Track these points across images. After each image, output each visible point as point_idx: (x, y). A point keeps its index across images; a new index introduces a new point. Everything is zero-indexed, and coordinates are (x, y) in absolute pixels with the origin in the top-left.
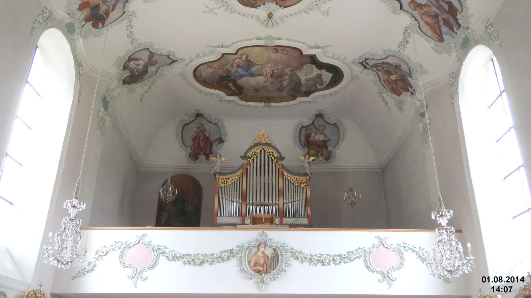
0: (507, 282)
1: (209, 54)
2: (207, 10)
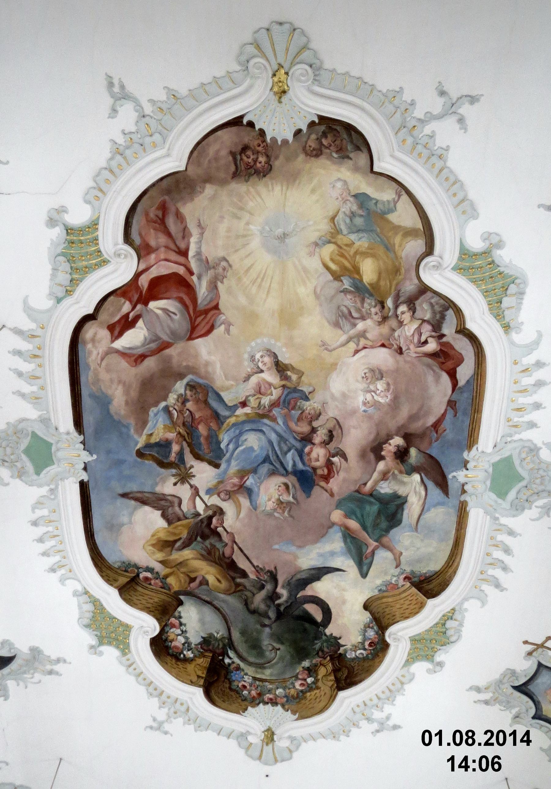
0: (487, 744)
1: (182, 597)
2: (155, 725)
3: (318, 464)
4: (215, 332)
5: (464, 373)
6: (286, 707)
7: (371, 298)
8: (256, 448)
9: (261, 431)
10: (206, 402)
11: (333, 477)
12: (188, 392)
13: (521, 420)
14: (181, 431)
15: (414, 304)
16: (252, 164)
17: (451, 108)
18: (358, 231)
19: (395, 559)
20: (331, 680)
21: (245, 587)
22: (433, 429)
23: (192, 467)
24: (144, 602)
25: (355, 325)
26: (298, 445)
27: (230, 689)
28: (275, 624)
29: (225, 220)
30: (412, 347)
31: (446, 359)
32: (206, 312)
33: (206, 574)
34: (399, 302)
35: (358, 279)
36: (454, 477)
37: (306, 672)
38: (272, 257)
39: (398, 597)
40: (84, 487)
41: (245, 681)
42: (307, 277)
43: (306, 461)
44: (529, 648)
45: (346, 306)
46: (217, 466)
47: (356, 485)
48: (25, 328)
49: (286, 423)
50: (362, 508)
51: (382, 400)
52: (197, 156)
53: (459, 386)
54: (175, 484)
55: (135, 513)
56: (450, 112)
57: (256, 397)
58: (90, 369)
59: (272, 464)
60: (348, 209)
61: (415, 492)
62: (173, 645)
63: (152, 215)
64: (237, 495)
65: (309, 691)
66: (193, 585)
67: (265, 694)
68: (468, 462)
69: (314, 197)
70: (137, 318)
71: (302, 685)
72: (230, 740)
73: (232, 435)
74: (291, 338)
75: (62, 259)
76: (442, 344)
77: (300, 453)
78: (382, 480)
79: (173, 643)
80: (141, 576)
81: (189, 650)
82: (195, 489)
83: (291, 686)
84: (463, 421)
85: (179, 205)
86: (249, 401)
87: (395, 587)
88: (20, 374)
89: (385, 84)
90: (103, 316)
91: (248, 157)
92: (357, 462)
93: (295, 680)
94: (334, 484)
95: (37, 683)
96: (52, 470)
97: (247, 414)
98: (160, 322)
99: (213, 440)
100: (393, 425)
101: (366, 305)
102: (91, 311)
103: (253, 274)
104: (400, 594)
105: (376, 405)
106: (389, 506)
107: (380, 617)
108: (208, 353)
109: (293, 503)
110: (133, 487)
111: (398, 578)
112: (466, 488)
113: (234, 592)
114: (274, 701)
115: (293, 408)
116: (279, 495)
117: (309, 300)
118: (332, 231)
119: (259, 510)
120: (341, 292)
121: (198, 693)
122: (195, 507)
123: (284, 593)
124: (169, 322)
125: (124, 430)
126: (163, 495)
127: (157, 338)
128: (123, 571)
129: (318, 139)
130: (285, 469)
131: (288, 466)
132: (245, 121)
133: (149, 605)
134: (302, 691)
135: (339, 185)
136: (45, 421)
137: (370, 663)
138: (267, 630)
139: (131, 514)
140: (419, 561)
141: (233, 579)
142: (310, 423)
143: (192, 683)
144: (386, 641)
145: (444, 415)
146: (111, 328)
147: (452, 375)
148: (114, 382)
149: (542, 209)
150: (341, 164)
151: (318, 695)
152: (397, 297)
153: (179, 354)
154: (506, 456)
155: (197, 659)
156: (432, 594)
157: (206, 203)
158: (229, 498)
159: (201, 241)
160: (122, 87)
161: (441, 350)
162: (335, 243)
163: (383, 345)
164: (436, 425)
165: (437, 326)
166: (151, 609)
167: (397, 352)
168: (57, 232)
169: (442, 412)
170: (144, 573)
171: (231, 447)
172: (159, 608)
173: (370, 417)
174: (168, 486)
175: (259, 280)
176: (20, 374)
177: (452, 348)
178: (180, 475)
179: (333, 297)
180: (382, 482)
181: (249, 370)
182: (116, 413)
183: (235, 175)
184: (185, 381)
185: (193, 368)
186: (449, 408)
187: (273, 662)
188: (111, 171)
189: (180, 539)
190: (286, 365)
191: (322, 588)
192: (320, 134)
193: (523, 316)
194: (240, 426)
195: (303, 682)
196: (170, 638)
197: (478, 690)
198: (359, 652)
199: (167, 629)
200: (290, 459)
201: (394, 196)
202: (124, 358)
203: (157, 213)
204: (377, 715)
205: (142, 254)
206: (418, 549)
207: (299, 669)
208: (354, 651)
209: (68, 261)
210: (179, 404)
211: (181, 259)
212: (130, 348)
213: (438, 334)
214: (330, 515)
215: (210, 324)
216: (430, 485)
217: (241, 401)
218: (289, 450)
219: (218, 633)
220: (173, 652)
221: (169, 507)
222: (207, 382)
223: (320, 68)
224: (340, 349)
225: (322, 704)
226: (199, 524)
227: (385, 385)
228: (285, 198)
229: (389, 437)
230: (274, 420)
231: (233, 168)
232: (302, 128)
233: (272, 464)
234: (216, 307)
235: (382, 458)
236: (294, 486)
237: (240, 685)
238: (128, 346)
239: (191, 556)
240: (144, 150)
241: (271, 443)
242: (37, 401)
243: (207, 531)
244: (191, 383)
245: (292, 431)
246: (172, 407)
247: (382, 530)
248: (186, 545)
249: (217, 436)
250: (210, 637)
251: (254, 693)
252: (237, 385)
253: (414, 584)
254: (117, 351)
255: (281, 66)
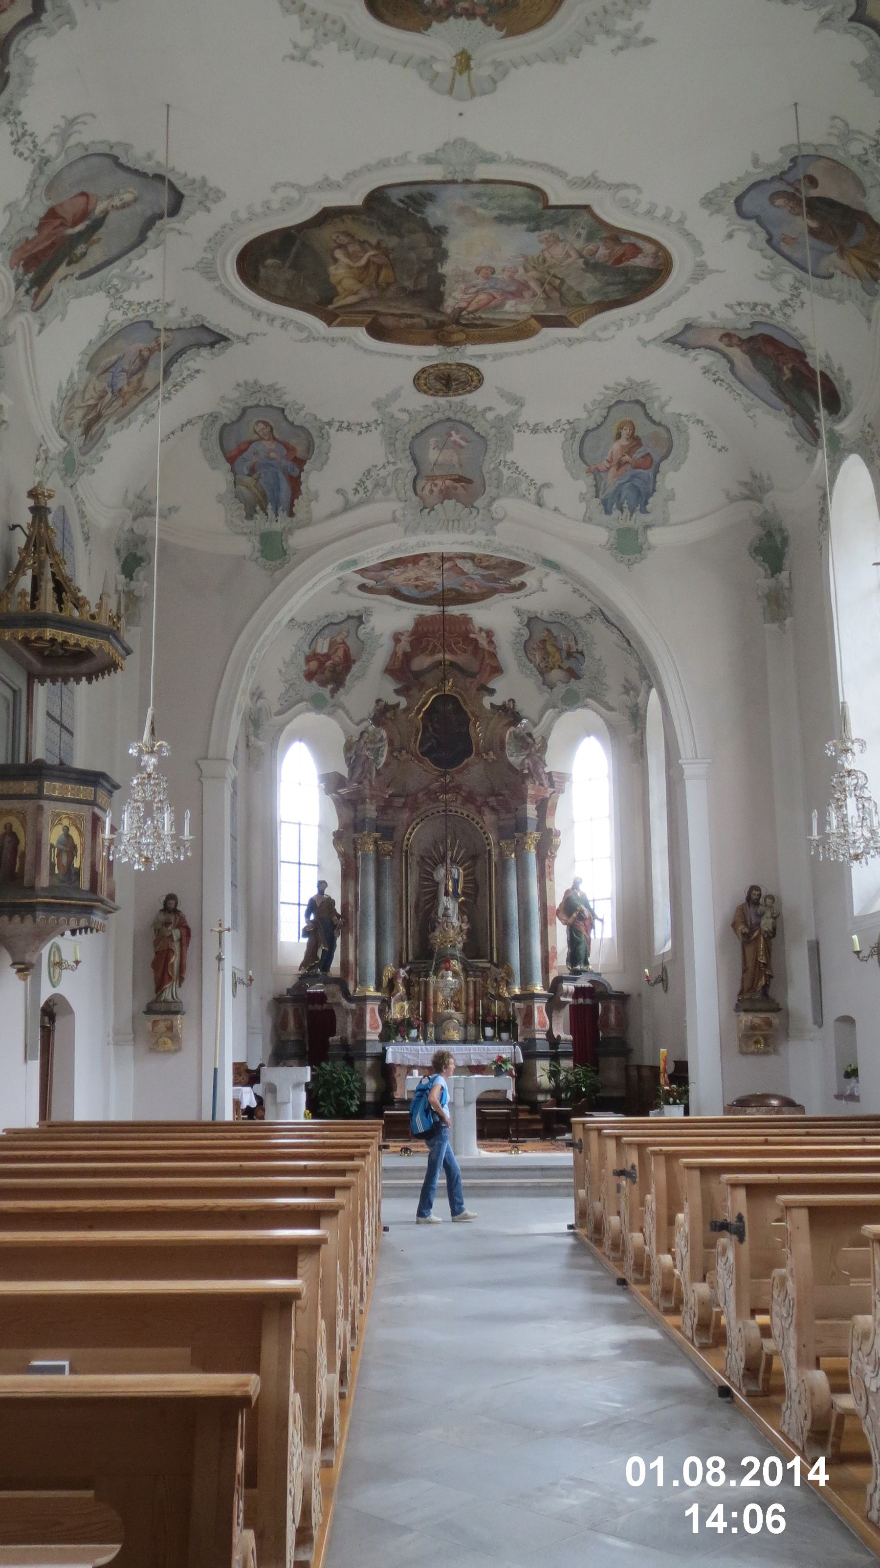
2: (297, 53)
6: (489, 19)
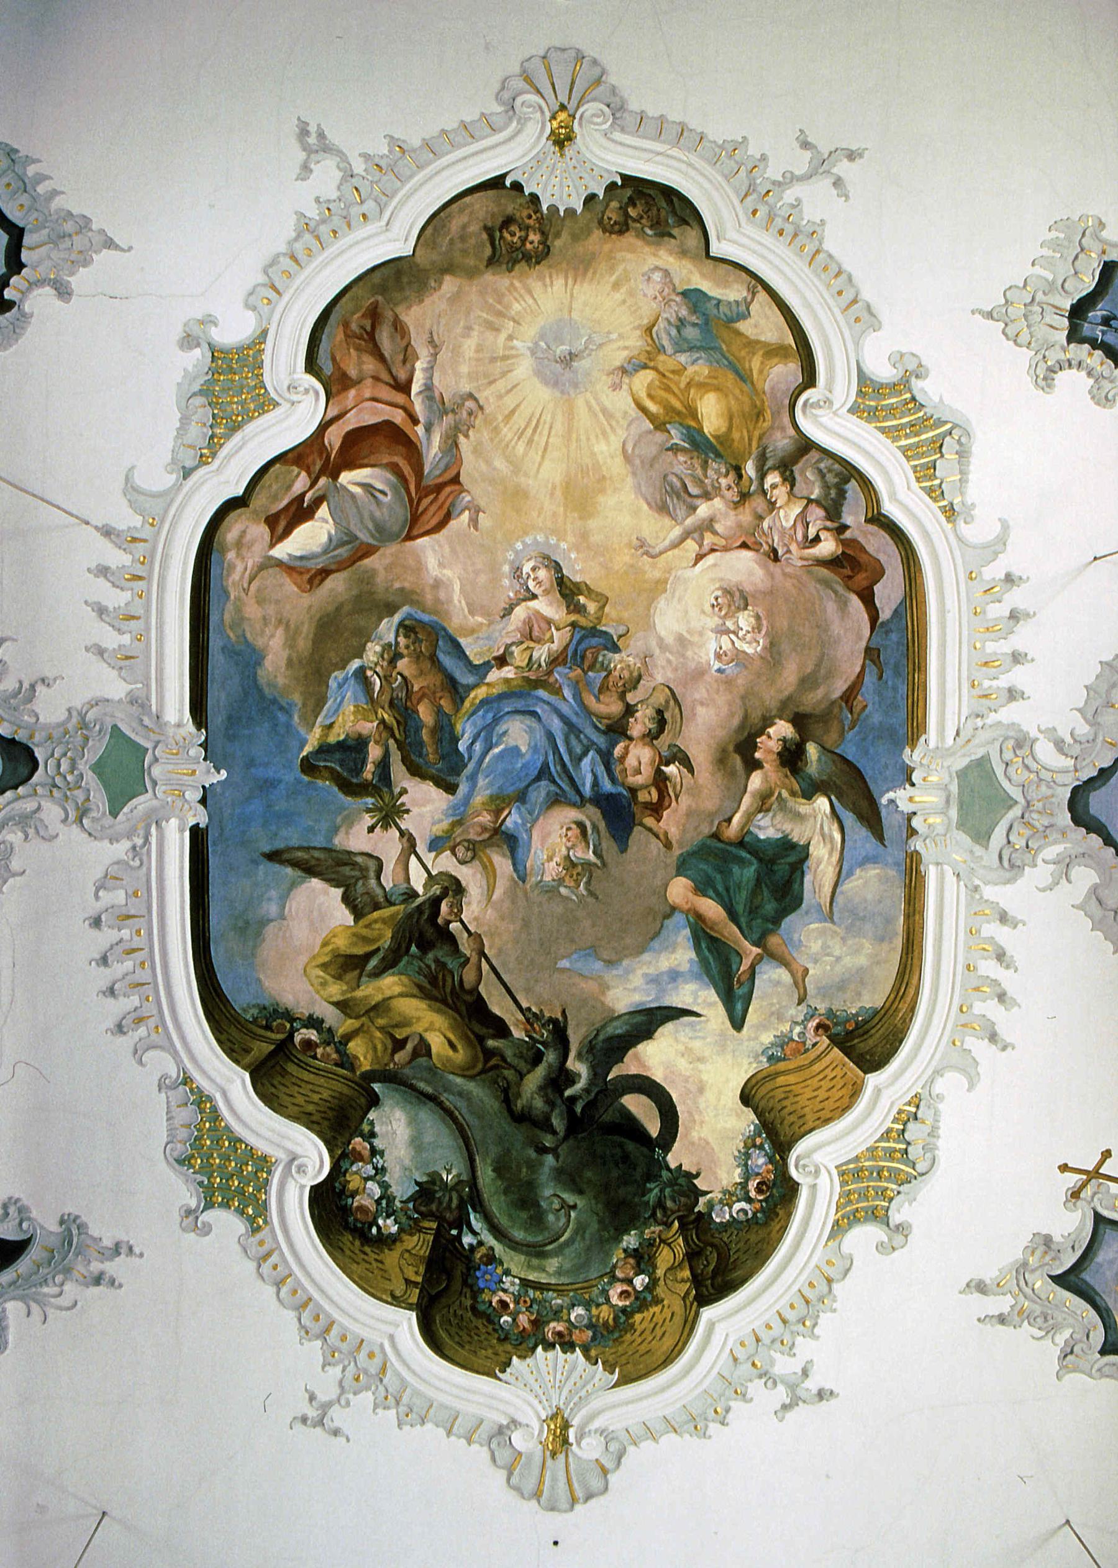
1: (377, 1087)
2: (312, 1413)
3: (639, 780)
4: (453, 523)
5: (889, 593)
6: (593, 1353)
7: (718, 460)
8: (523, 749)
9: (534, 714)
10: (433, 659)
11: (670, 805)
12: (402, 640)
13: (995, 683)
14: (386, 716)
15: (792, 471)
16: (519, 244)
17: (820, 166)
18: (690, 349)
19: (796, 983)
20: (683, 1281)
21: (504, 1059)
22: (844, 704)
23: (404, 791)
24: (300, 1100)
25: (694, 509)
26: (601, 741)
27: (474, 1309)
28: (565, 1146)
29: (475, 333)
30: (793, 547)
31: (852, 568)
32: (439, 488)
33: (426, 1030)
34: (766, 468)
35: (694, 428)
36: (892, 801)
37: (632, 1261)
38: (550, 395)
39: (806, 1073)
40: (198, 836)
41: (505, 1291)
42: (607, 424)
43: (617, 773)
44: (1073, 1179)
45: (677, 475)
46: (451, 789)
47: (712, 822)
48: (122, 527)
49: (578, 696)
50: (725, 873)
51: (750, 650)
52: (433, 235)
53: (880, 620)
54: (371, 829)
55: (292, 893)
56: (821, 171)
57: (524, 646)
58: (228, 597)
59: (554, 782)
60: (674, 315)
61: (823, 835)
62: (355, 1204)
63: (354, 326)
64: (488, 851)
65: (640, 1311)
66: (401, 1057)
67: (548, 1322)
68: (913, 770)
69: (618, 296)
70: (318, 502)
71: (624, 1294)
72: (475, 1447)
73: (480, 723)
74: (584, 535)
75: (200, 400)
76: (845, 543)
77: (606, 758)
78: (760, 812)
79: (358, 1198)
80: (298, 1038)
81: (388, 1217)
82: (408, 840)
83: (601, 1300)
84: (895, 689)
85: (399, 310)
86: (512, 653)
87: (802, 1048)
88: (101, 611)
89: (719, 131)
90: (259, 501)
91: (513, 235)
92: (712, 775)
93: (610, 1283)
94: (671, 822)
95: (68, 1309)
96: (141, 804)
97: (507, 681)
98: (357, 507)
99: (445, 733)
100: (771, 697)
101: (710, 472)
102: (240, 492)
103: (519, 420)
104: (812, 1063)
105: (739, 657)
106: (776, 868)
107: (776, 1126)
108: (440, 566)
109: (595, 865)
110: (290, 837)
111: (805, 1028)
112: (915, 823)
113: (483, 1071)
114: (567, 1339)
115: (591, 667)
116: (569, 849)
117: (616, 466)
118: (648, 349)
119: (532, 880)
120: (668, 449)
121: (407, 1322)
122: (408, 880)
123: (578, 1066)
124: (373, 507)
125: (282, 717)
126: (349, 853)
127: (350, 538)
128: (261, 1027)
129: (621, 208)
130: (578, 792)
131: (584, 784)
132: (508, 183)
133: (311, 1108)
134: (624, 1310)
135: (657, 276)
136: (139, 702)
137: (762, 1233)
138: (550, 1159)
139: (284, 898)
140: (842, 986)
141: (481, 1040)
142: (622, 696)
143: (396, 1301)
144: (791, 1178)
145: (861, 675)
146: (271, 521)
147: (868, 598)
148: (273, 624)
149: (978, 316)
150: (658, 244)
151: (659, 1319)
152: (762, 459)
153: (388, 568)
154: (978, 756)
155: (405, 1237)
156: (873, 1062)
157: (443, 306)
158: (473, 858)
159: (432, 367)
160: (321, 135)
161: (843, 553)
162: (655, 369)
163: (744, 546)
164: (849, 696)
165: (833, 510)
166: (314, 1118)
167: (769, 557)
168: (198, 356)
169: (858, 669)
170: (303, 1031)
171: (478, 747)
172: (330, 1114)
173: (729, 683)
174: (358, 838)
175: (530, 431)
176: (101, 611)
177: (863, 549)
178: (380, 810)
179: (655, 459)
180: (760, 816)
181: (511, 595)
182: (269, 685)
183: (492, 262)
184: (397, 618)
185: (413, 592)
186: (867, 662)
187: (562, 1239)
188: (293, 258)
189: (378, 949)
190: (577, 585)
191: (655, 1057)
192: (626, 200)
193: (973, 493)
194: (495, 705)
195: (625, 1287)
196: (352, 1186)
197: (981, 1288)
198: (737, 1206)
199: (345, 1165)
200: (588, 770)
201: (745, 294)
202: (290, 575)
203: (363, 326)
204: (784, 1366)
205: (334, 390)
206: (838, 959)
207: (617, 1256)
208: (727, 1204)
209: (210, 404)
210: (385, 664)
211: (400, 398)
212: (301, 558)
213: (836, 525)
214: (667, 885)
215: (444, 510)
216: (849, 818)
217: (496, 654)
218: (585, 753)
219: (449, 1172)
220: (356, 1220)
221: (358, 880)
222: (435, 618)
223: (622, 108)
224: (670, 553)
225: (668, 1342)
226: (416, 917)
227: (752, 620)
228: (572, 295)
229: (767, 722)
230: (557, 691)
231: (488, 251)
232: (596, 192)
233: (554, 782)
234: (456, 480)
235: (756, 765)
236: (595, 828)
237: (495, 1300)
238: (298, 554)
239: (397, 989)
240: (349, 226)
241: (551, 737)
242: (127, 662)
243: (430, 932)
244: (407, 623)
245: (588, 712)
246: (371, 668)
247: (766, 919)
248: (389, 964)
249: (452, 727)
250: (432, 1182)
251: (524, 1320)
252: (490, 623)
253: (835, 1040)
254: (279, 563)
255: (563, 107)
